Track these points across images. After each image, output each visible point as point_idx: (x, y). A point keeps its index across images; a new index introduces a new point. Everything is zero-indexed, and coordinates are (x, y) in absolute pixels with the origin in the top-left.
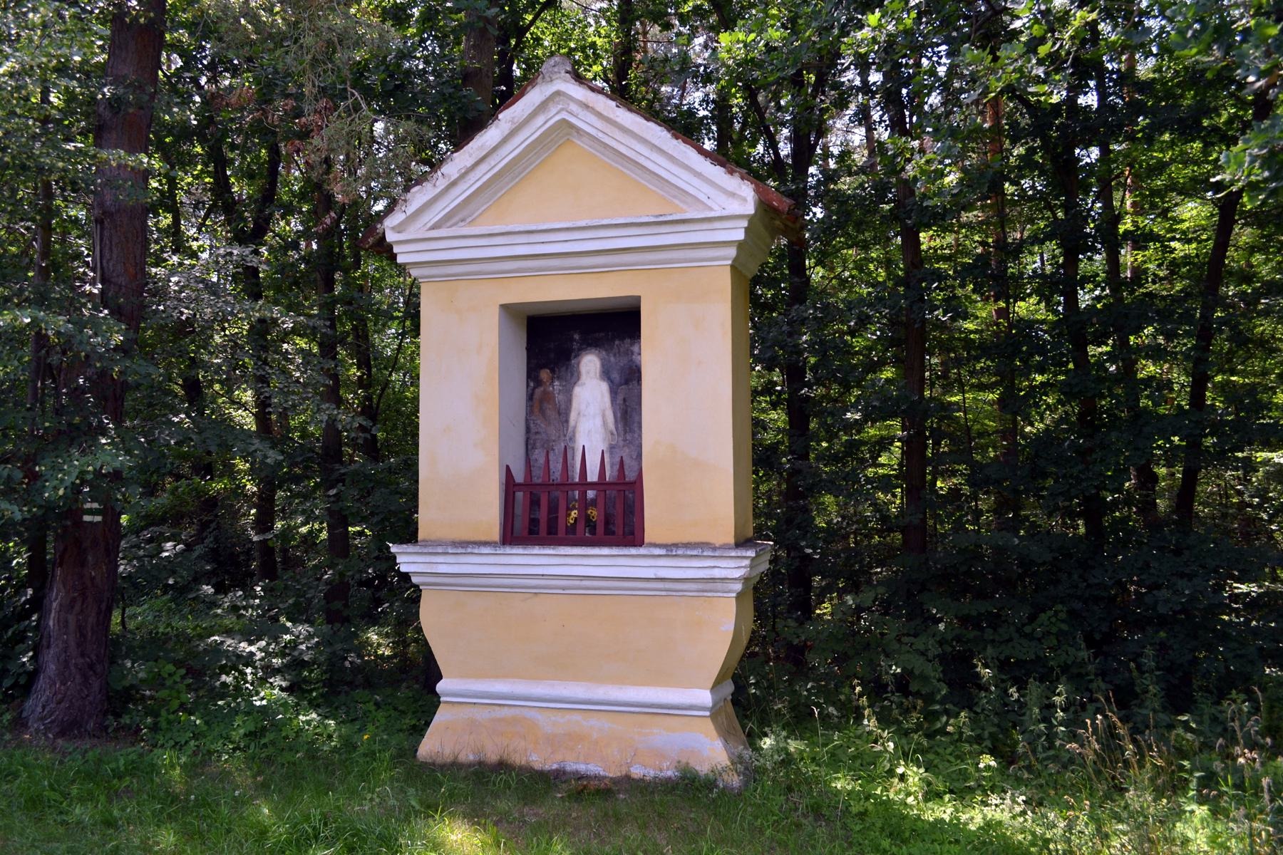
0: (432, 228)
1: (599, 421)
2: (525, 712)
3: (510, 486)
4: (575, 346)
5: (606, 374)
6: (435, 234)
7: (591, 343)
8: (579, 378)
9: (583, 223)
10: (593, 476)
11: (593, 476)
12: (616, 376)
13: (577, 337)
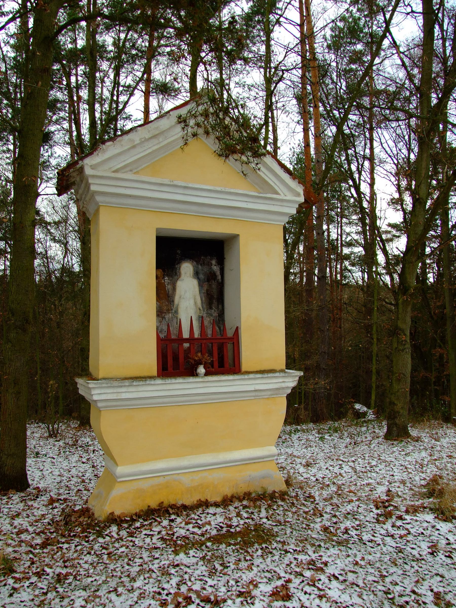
0: (114, 172)
1: (192, 302)
2: (175, 476)
3: (159, 340)
4: (178, 257)
5: (196, 274)
6: (113, 175)
7: (187, 257)
8: (180, 276)
9: (219, 189)
10: (186, 335)
11: (186, 335)
12: (201, 276)
13: (179, 252)
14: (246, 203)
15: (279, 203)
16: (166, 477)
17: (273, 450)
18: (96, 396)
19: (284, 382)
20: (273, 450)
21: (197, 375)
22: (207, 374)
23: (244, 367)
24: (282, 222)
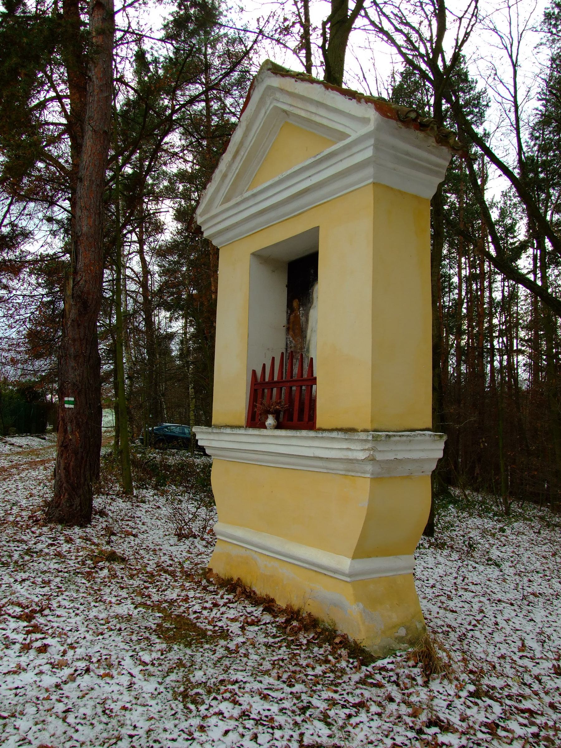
14: (309, 180)
15: (346, 154)
16: (248, 551)
17: (345, 563)
18: (203, 441)
19: (348, 449)
20: (345, 563)
21: (265, 427)
22: (279, 426)
23: (320, 422)
24: (368, 179)
